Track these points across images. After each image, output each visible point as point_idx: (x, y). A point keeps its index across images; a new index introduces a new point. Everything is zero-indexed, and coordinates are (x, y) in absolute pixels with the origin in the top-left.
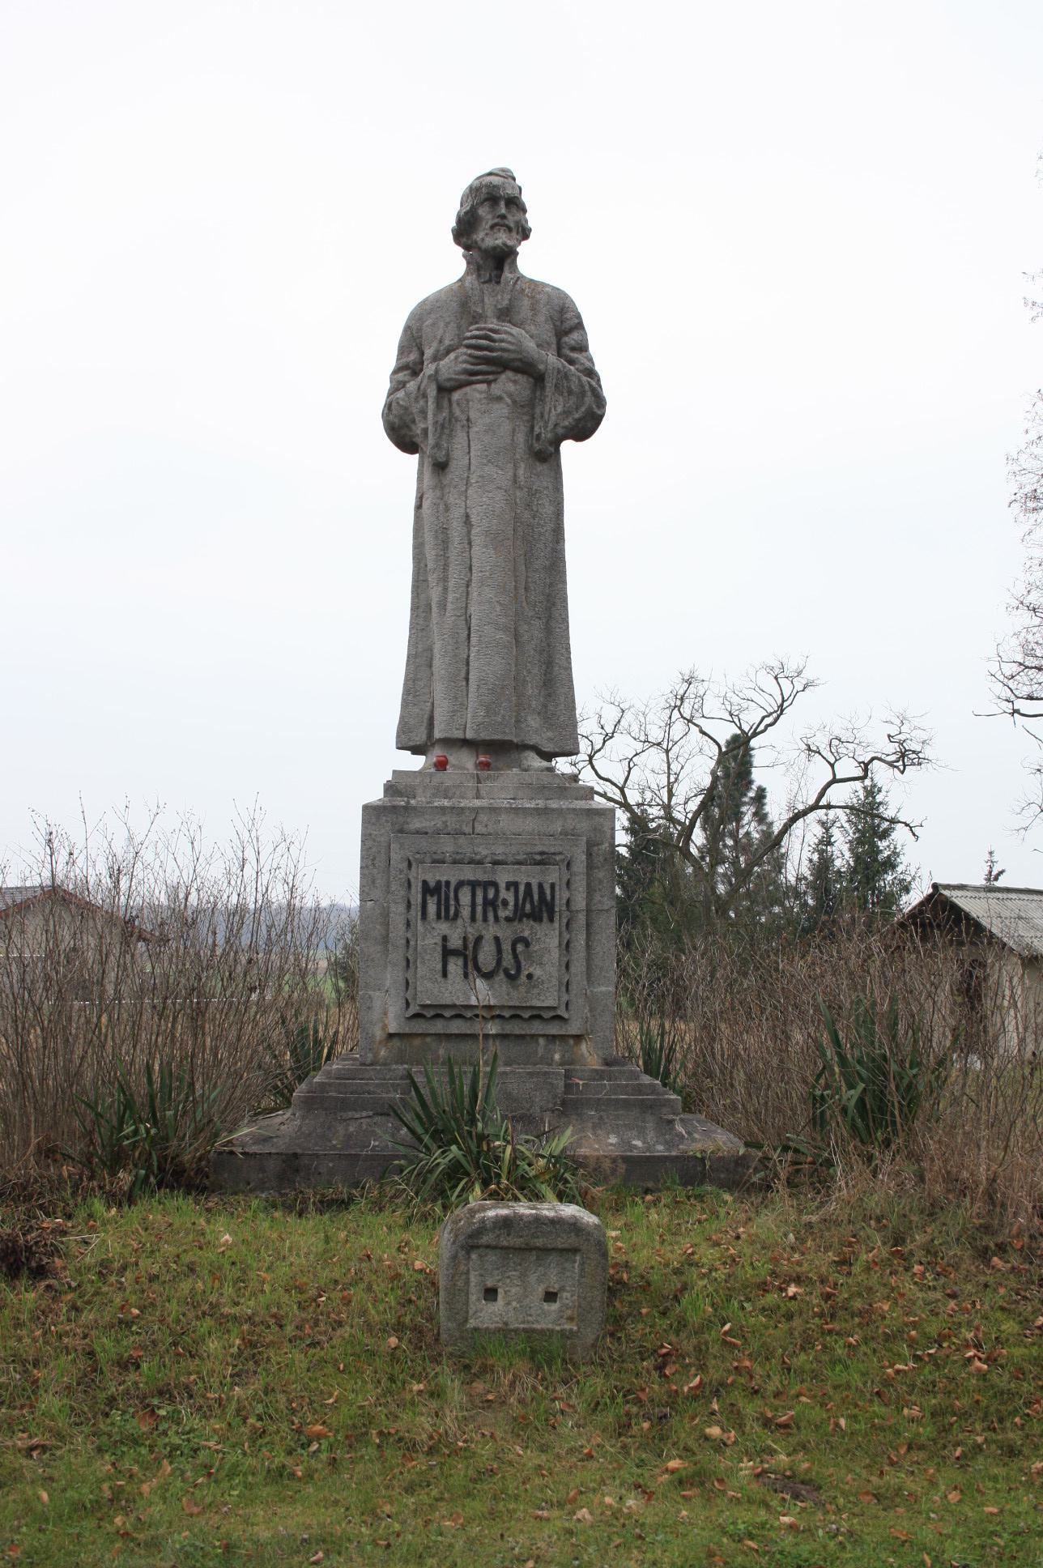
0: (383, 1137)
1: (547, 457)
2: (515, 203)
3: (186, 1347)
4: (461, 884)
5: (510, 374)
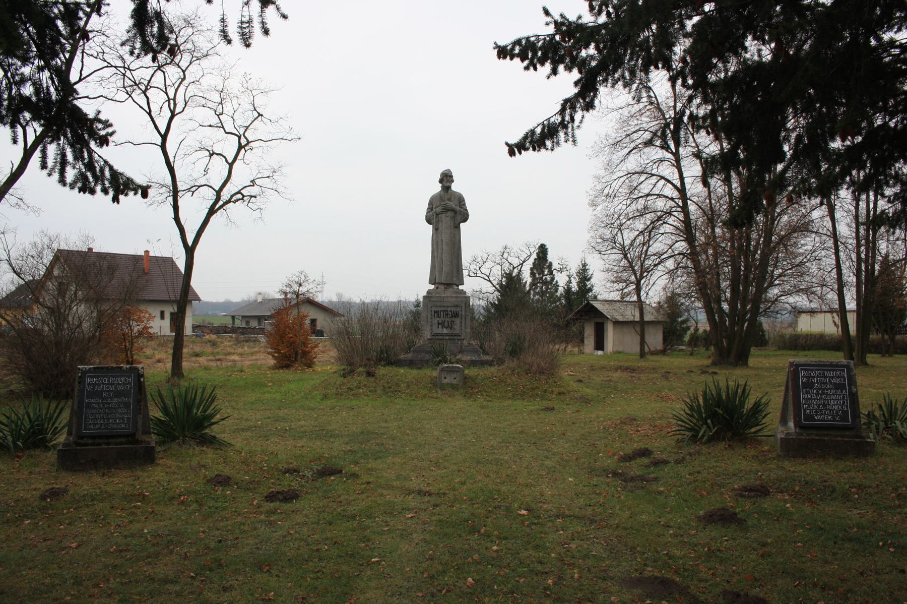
0: (427, 357)
1: (458, 227)
2: (451, 176)
3: (398, 385)
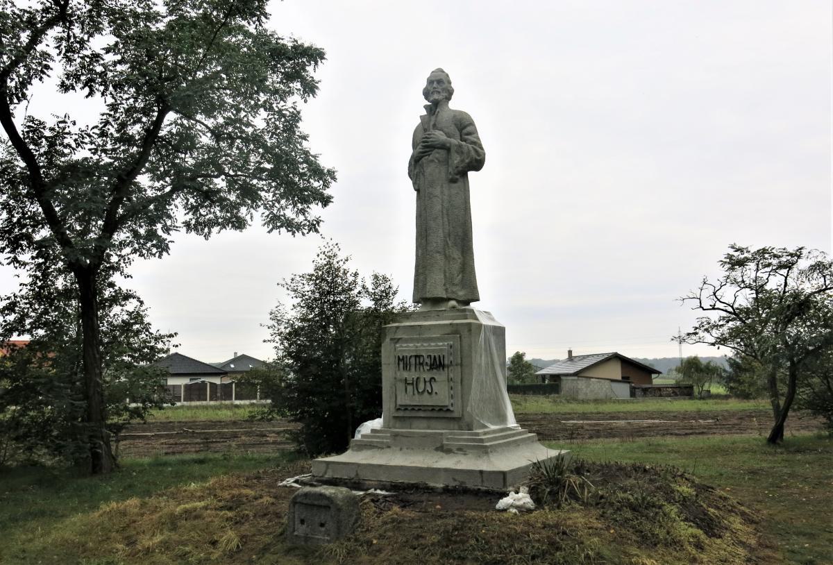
4: (411, 357)
5: (436, 150)
